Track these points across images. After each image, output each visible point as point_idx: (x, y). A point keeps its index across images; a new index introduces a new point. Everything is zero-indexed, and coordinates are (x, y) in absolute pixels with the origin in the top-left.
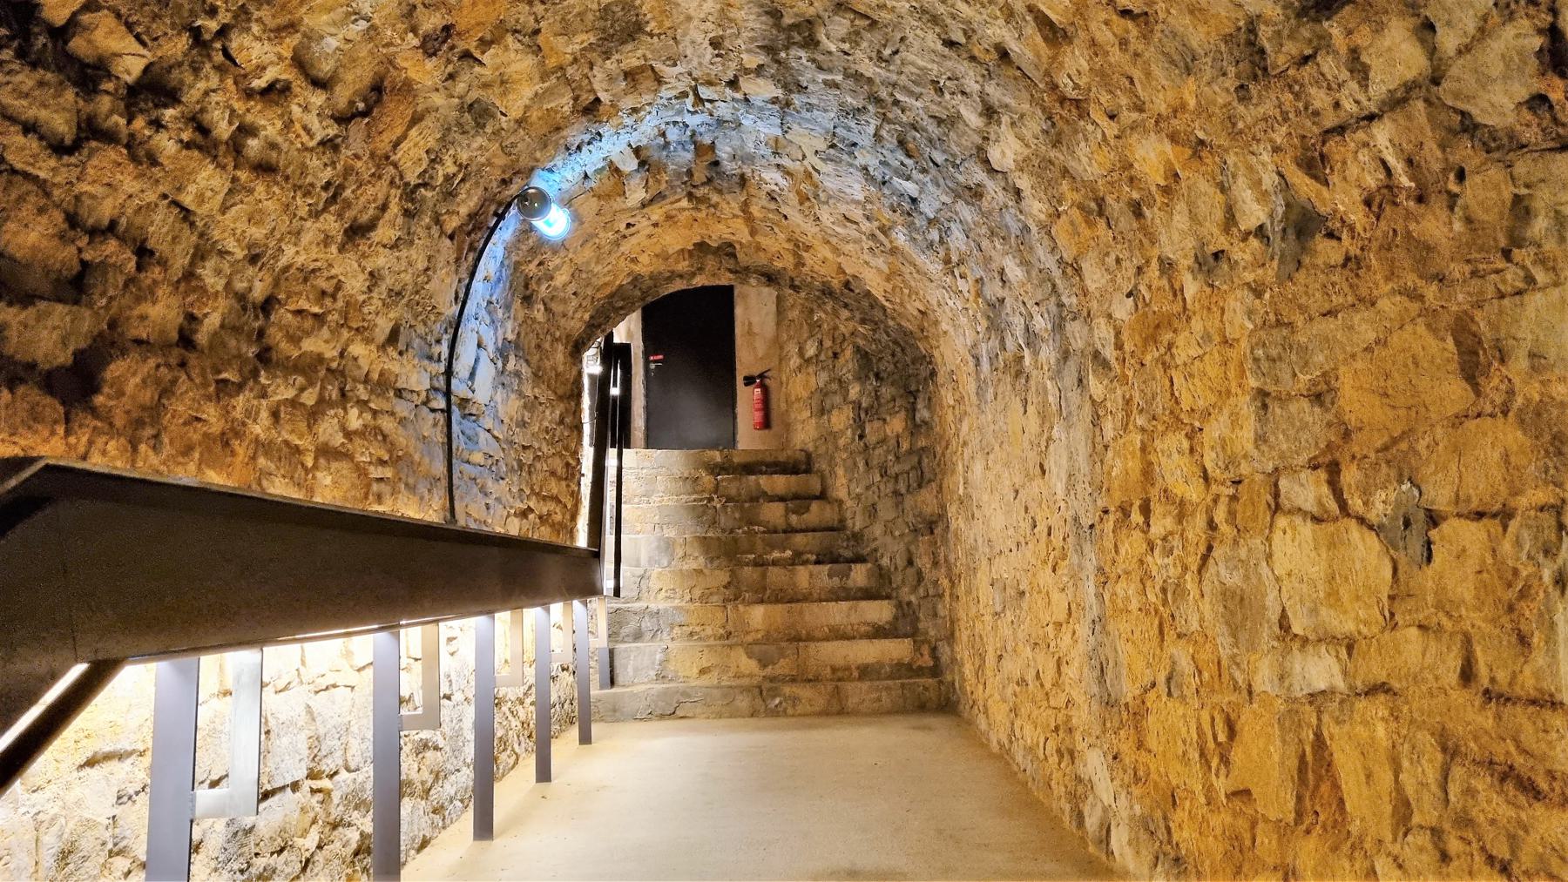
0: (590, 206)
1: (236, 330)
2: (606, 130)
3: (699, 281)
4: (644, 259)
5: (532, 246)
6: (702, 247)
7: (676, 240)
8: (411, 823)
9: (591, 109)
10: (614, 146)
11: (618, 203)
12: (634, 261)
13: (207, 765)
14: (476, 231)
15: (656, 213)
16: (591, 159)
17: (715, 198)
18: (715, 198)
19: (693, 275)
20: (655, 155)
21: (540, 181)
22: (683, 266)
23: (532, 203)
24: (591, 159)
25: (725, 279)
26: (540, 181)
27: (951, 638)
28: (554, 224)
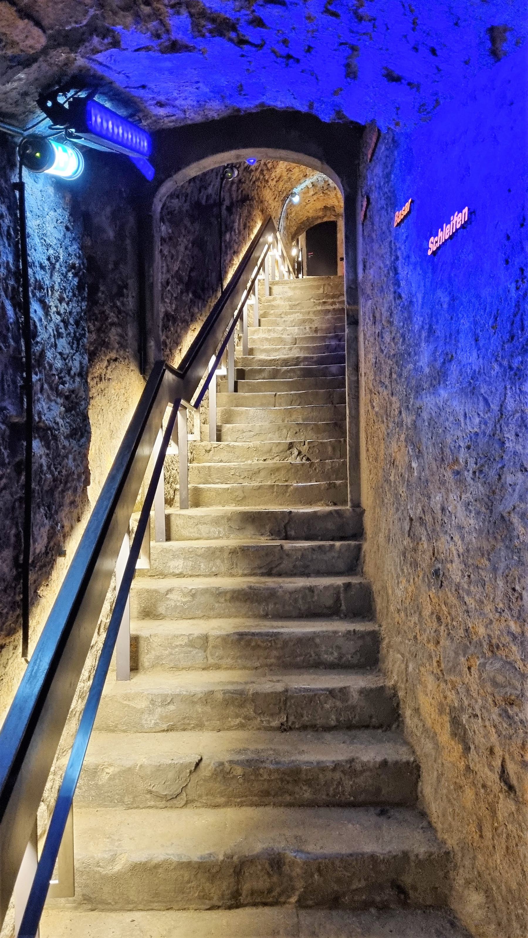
0: (302, 195)
1: (79, 441)
2: (307, 179)
3: (325, 219)
4: (311, 211)
5: (291, 205)
6: (325, 207)
7: (320, 205)
8: (65, 740)
9: (305, 176)
10: (308, 182)
11: (307, 195)
12: (308, 212)
13: (115, 673)
14: (284, 200)
15: (315, 197)
16: (303, 185)
17: (329, 193)
18: (329, 193)
19: (323, 217)
20: (315, 184)
21: (295, 190)
22: (321, 214)
23: (293, 194)
24: (303, 185)
25: (333, 219)
26: (295, 190)
27: (184, 549)
28: (296, 199)
